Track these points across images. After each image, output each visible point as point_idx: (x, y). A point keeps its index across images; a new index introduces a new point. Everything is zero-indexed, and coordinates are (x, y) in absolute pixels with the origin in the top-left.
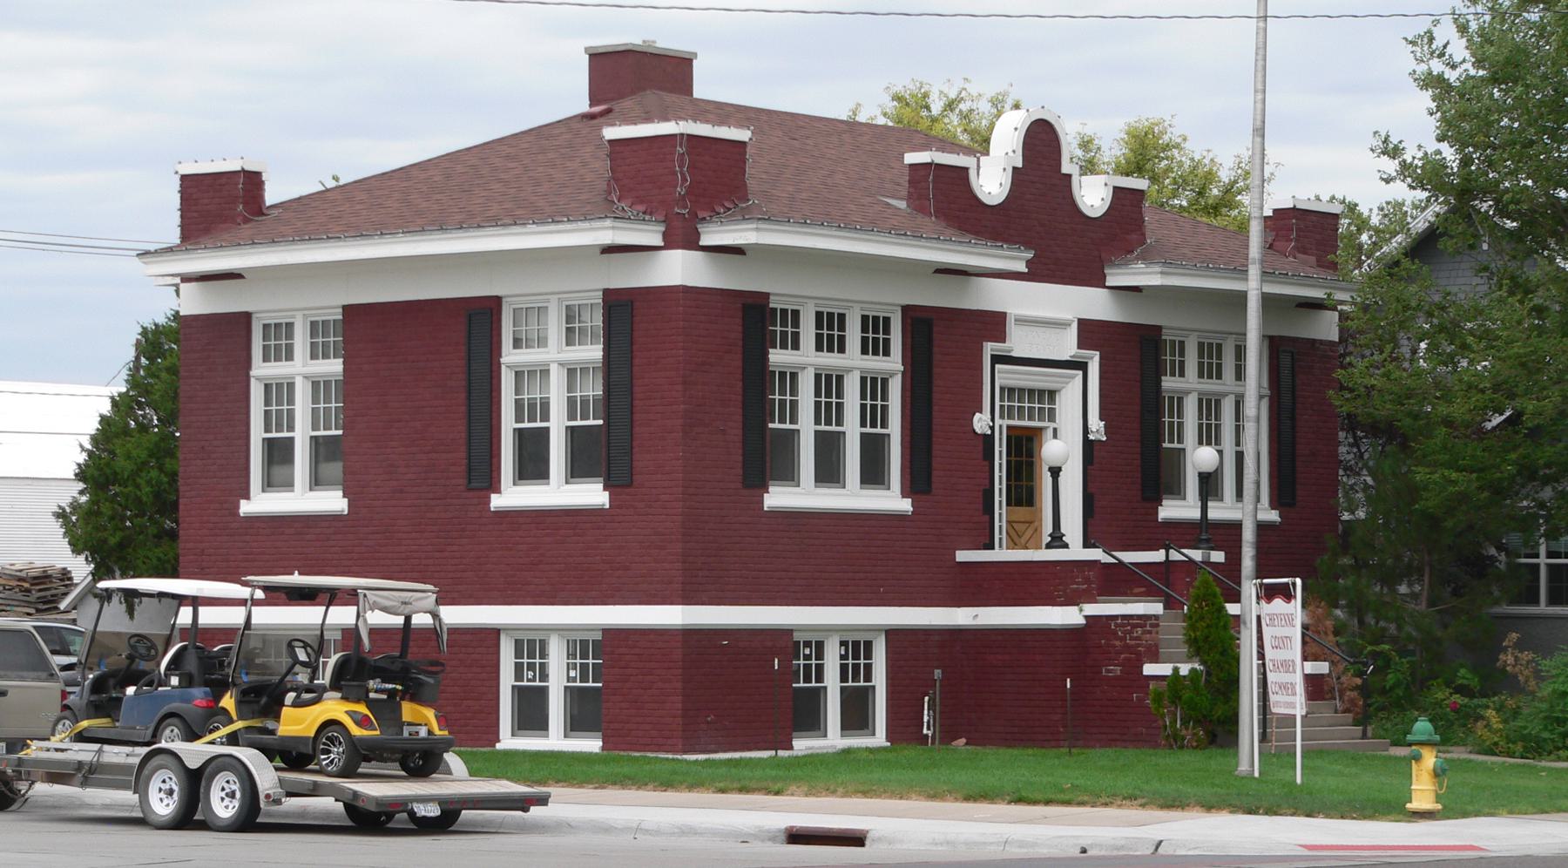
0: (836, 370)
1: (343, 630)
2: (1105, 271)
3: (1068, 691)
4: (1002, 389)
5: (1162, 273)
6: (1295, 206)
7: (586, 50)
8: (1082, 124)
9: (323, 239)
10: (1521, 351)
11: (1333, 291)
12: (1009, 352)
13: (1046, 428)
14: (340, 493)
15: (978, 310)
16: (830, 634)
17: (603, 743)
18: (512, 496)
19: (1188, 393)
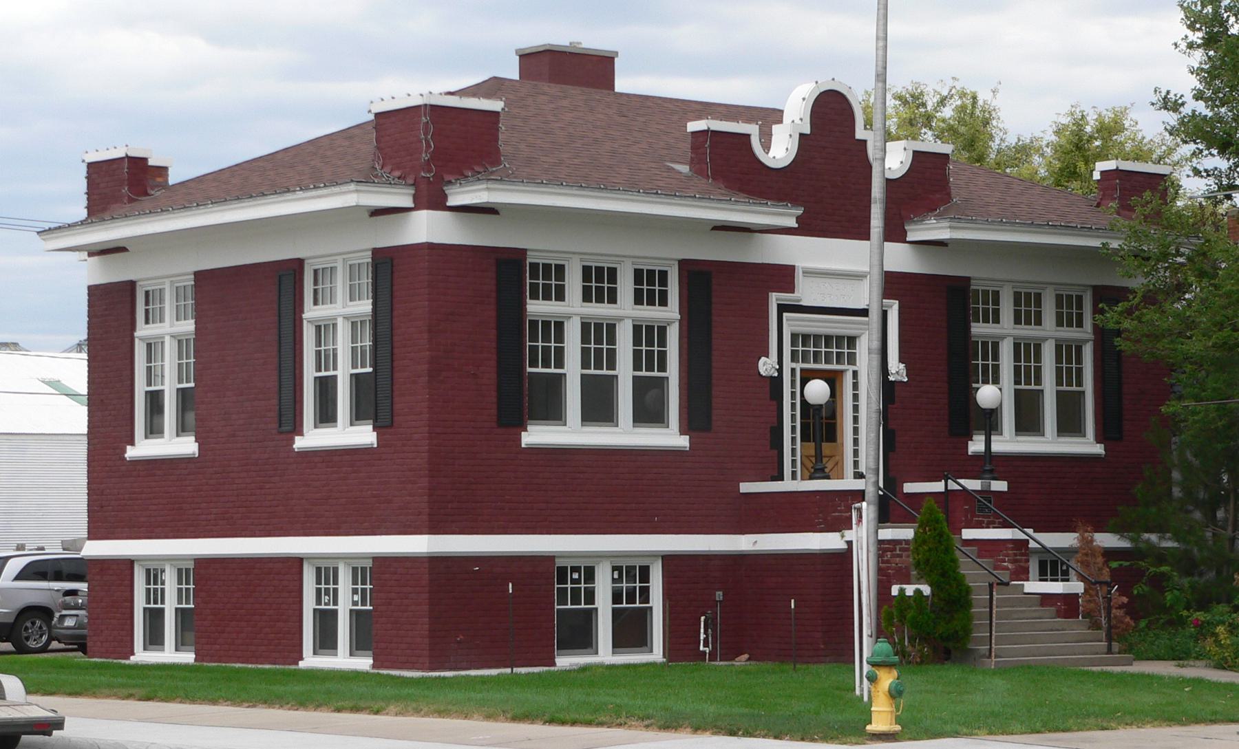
0: (606, 319)
1: (195, 559)
2: (906, 228)
3: (793, 612)
4: (794, 337)
5: (950, 227)
6: (709, 128)
7: (517, 51)
8: (1057, 114)
9: (158, 212)
10: (1234, 288)
11: (1109, 241)
12: (799, 301)
13: (846, 370)
14: (193, 438)
15: (763, 264)
17: (374, 661)
18: (313, 438)
19: (1003, 337)
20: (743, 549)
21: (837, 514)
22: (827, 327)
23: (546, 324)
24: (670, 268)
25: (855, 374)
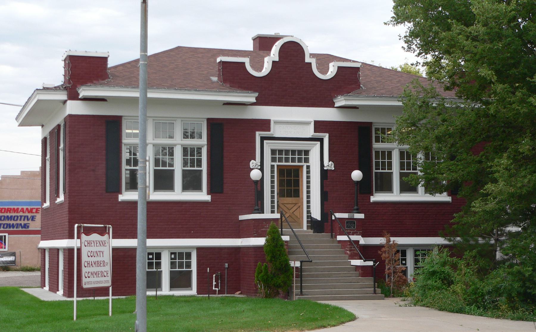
0: (190, 146)
2: (334, 101)
5: (345, 100)
6: (221, 61)
12: (273, 135)
16: (163, 249)
20: (239, 245)
21: (264, 229)
22: (296, 147)
23: (383, 153)
24: (203, 122)
25: (308, 167)
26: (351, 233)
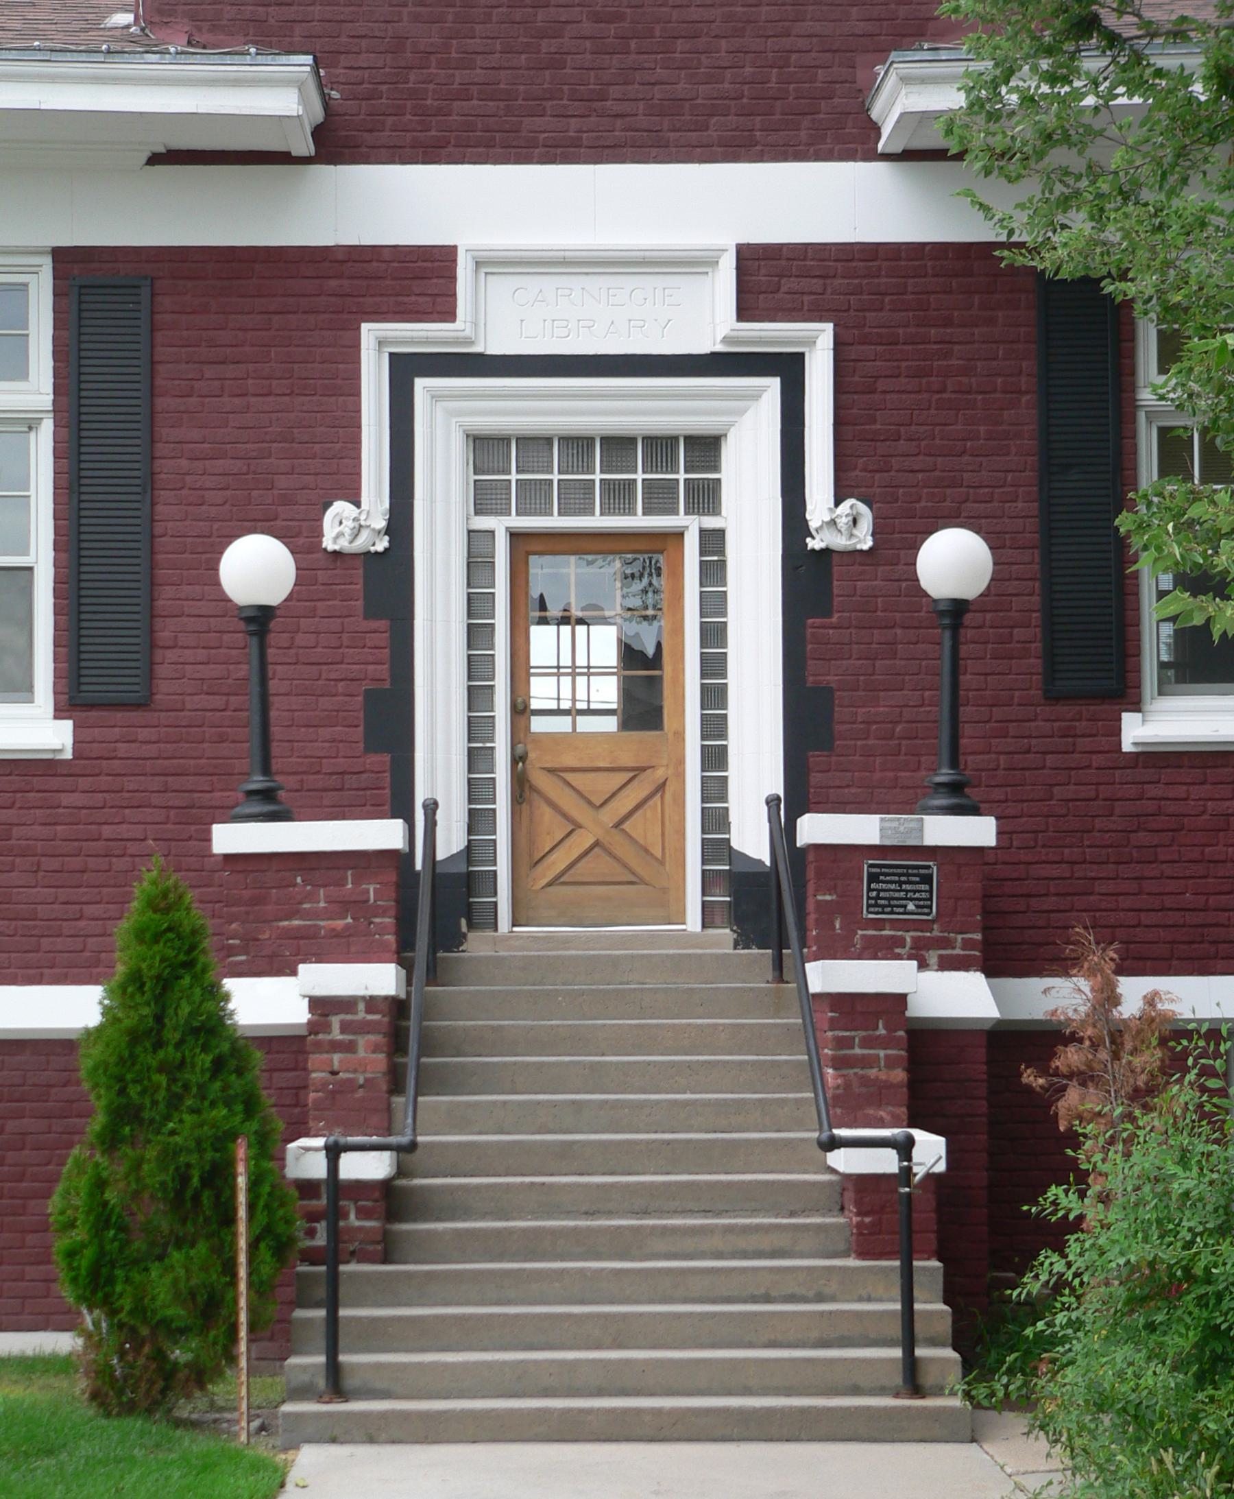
21: (296, 922)
25: (713, 541)
26: (901, 942)
